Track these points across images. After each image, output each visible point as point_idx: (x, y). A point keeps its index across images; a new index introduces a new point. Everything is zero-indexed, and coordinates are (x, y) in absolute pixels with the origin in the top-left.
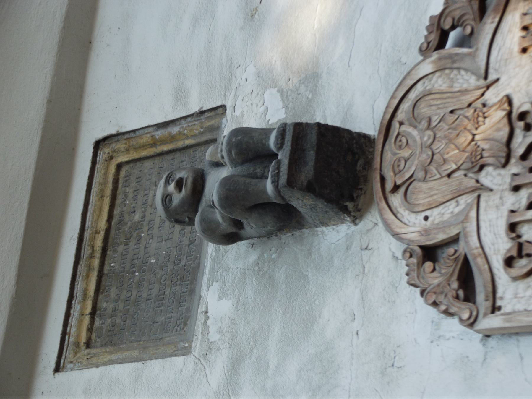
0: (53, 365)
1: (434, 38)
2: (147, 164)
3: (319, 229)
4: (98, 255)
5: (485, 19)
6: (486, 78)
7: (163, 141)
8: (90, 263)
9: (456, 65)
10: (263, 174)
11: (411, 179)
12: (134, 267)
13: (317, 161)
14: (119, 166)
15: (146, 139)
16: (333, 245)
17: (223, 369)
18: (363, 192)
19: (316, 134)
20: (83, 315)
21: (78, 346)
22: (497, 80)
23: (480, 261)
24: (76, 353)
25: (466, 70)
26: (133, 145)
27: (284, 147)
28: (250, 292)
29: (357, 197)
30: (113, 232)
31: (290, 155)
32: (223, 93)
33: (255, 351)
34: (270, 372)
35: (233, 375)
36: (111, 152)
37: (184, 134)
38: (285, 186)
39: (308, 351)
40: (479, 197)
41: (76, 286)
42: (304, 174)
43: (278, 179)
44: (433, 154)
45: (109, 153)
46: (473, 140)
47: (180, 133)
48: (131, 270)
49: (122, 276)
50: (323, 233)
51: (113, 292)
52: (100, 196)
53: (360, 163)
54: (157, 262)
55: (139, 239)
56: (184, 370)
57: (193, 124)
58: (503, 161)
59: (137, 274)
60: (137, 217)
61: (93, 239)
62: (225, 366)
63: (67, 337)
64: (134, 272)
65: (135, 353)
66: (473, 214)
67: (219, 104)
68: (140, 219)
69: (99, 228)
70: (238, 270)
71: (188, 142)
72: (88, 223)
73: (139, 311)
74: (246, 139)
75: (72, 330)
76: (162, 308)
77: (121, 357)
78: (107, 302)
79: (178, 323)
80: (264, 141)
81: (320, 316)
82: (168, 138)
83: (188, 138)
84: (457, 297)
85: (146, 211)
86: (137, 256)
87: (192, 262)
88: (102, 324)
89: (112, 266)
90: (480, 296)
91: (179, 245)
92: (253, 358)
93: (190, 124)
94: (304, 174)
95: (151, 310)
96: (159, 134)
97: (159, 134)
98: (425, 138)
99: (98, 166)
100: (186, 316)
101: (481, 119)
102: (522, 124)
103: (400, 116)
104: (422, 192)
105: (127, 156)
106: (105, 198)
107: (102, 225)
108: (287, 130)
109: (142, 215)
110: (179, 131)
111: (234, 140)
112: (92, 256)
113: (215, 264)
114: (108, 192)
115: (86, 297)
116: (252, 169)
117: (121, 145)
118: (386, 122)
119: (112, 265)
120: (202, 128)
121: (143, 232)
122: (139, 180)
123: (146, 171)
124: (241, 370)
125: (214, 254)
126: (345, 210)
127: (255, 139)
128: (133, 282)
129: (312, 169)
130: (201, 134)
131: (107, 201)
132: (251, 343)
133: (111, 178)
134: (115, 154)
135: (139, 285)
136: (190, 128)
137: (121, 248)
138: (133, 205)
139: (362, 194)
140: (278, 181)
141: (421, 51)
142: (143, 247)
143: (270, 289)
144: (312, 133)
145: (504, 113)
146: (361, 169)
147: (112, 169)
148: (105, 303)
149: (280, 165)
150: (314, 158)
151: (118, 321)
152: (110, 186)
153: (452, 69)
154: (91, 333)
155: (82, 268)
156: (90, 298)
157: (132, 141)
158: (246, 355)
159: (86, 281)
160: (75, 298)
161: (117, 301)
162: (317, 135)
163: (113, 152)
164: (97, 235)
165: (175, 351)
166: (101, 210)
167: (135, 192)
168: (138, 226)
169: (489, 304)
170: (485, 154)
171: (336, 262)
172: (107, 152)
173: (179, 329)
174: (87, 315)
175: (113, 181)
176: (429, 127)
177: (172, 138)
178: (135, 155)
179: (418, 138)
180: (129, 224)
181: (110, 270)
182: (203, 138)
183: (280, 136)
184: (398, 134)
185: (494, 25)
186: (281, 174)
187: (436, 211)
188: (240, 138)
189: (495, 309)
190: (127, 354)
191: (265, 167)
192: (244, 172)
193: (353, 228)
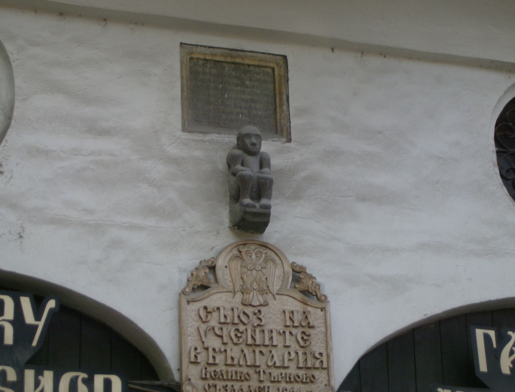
0: (183, 42)
1: (298, 269)
2: (271, 86)
4: (232, 60)
5: (300, 294)
6: (277, 294)
7: (281, 99)
9: (285, 280)
11: (242, 259)
14: (273, 69)
15: (284, 90)
22: (275, 299)
23: (207, 295)
25: (282, 285)
40: (231, 292)
44: (251, 270)
46: (254, 289)
47: (283, 111)
51: (214, 71)
58: (244, 303)
60: (248, 83)
61: (239, 56)
66: (225, 290)
72: (248, 54)
75: (199, 49)
83: (280, 115)
84: (194, 285)
90: (194, 296)
96: (284, 97)
97: (284, 97)
98: (258, 266)
101: (262, 293)
102: (256, 311)
103: (269, 252)
104: (236, 264)
107: (247, 62)
114: (262, 64)
117: (282, 73)
118: (267, 246)
125: (224, 142)
126: (234, 226)
130: (281, 124)
131: (257, 63)
133: (268, 64)
137: (234, 74)
141: (293, 263)
145: (262, 303)
147: (272, 65)
153: (284, 278)
169: (190, 300)
170: (248, 295)
176: (262, 268)
177: (281, 105)
178: (277, 80)
179: (258, 262)
180: (245, 78)
182: (278, 125)
184: (262, 253)
185: (296, 298)
187: (228, 271)
189: (188, 302)
190: (185, 89)
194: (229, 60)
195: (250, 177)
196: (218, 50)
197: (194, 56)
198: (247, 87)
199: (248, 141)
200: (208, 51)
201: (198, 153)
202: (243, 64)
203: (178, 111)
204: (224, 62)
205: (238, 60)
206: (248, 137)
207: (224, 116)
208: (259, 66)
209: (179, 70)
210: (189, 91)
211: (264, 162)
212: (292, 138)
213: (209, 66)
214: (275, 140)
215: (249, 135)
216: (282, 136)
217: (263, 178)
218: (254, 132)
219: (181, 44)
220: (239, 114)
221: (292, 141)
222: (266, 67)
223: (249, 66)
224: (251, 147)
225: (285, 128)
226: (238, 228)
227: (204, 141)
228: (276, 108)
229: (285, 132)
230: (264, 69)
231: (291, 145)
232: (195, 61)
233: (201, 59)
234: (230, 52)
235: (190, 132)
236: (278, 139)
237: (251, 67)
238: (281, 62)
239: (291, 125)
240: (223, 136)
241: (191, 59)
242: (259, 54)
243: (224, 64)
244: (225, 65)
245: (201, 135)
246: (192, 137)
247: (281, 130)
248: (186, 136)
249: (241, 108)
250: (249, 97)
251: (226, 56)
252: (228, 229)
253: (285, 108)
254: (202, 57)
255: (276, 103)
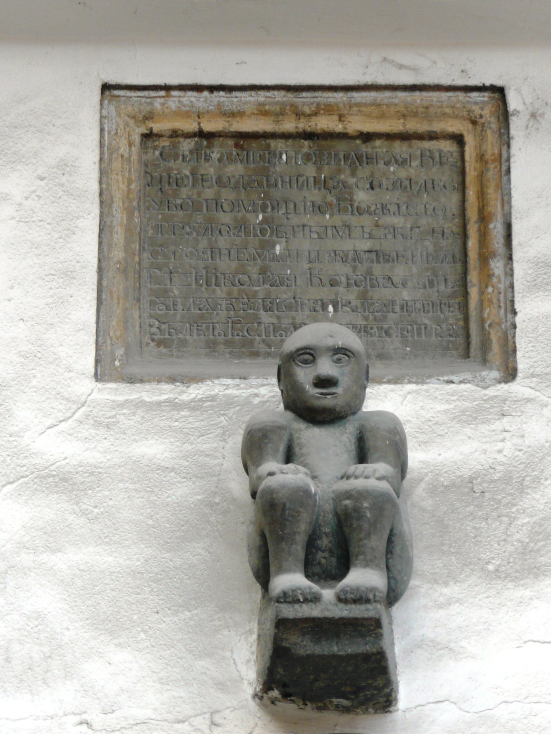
0: (113, 79)
2: (455, 198)
3: (256, 626)
4: (303, 125)
8: (287, 114)
10: (320, 549)
12: (273, 208)
13: (323, 657)
15: (495, 207)
16: (229, 654)
17: (63, 456)
18: (303, 706)
19: (365, 652)
20: (199, 117)
21: (147, 119)
24: (134, 117)
26: (488, 170)
27: (341, 605)
28: (179, 493)
29: (291, 700)
30: (342, 147)
31: (325, 618)
32: (538, 370)
33: (82, 520)
34: (44, 557)
35: (51, 479)
36: (482, 120)
37: (487, 287)
38: (277, 616)
39: (68, 629)
41: (248, 93)
42: (300, 640)
43: (289, 602)
45: (481, 116)
48: (268, 203)
49: (260, 184)
50: (251, 632)
51: (236, 170)
52: (405, 112)
53: (345, 702)
54: (275, 258)
55: (319, 209)
56: (71, 374)
57: (502, 305)
59: (261, 217)
61: (329, 109)
62: (67, 461)
63: (163, 93)
64: (264, 209)
65: (118, 254)
67: (522, 364)
68: (356, 205)
69: (350, 118)
70: (221, 460)
71: (474, 292)
72: (357, 96)
73: (195, 234)
74: (366, 526)
75: (175, 100)
76: (194, 286)
77: (115, 223)
78: (220, 160)
79: (163, 326)
80: (361, 557)
81: (119, 645)
82: (487, 249)
83: (482, 293)
85: (371, 214)
86: (292, 211)
87: (264, 337)
88: (183, 156)
89: (281, 157)
91: (296, 302)
92: (71, 518)
93: (502, 296)
94: (300, 640)
95: (193, 262)
97: (496, 228)
99: (461, 95)
100: (173, 341)
105: (474, 155)
106: (402, 121)
107: (357, 124)
108: (369, 606)
109: (364, 206)
110: (493, 275)
111: (366, 505)
112: (299, 115)
113: (238, 408)
115: (229, 117)
116: (327, 530)
119: (284, 157)
120: (490, 325)
121: (332, 215)
122: (430, 186)
123: (443, 200)
124: (55, 496)
125: (256, 401)
127: (366, 541)
128: (247, 211)
129: (308, 652)
130: (482, 321)
132: (96, 510)
133: (437, 127)
134: (479, 128)
135: (242, 226)
136: (495, 301)
137: (310, 171)
138: (384, 183)
139: (299, 706)
140: (285, 602)
142: (305, 221)
143: (178, 534)
144: (366, 644)
146: (335, 703)
148: (218, 156)
149: (311, 601)
150: (326, 653)
151: (184, 192)
152: (422, 127)
154: (171, 136)
155: (279, 96)
156: (227, 124)
157: (496, 167)
158: (77, 503)
159: (255, 111)
160: (229, 95)
161: (219, 182)
162: (363, 654)
163: (483, 124)
164: (336, 118)
165: (111, 338)
166: (382, 116)
167: (407, 183)
168: (345, 203)
171: (202, 664)
172: (483, 113)
173: (154, 330)
174: (199, 124)
175: (433, 132)
177: (485, 259)
180: (352, 181)
181: (275, 155)
183: (358, 596)
186: (297, 606)
188: (369, 515)
191: (330, 551)
192: (324, 516)
193: (250, 691)
194: (289, 125)
195: (302, 496)
196: (245, 96)
197: (157, 127)
198: (360, 211)
199: (304, 376)
200: (200, 101)
201: (155, 449)
202: (343, 136)
203: (85, 311)
204: (273, 136)
205: (324, 123)
206: (305, 362)
207: (266, 318)
208: (405, 137)
209: (95, 175)
210: (136, 246)
211: (379, 443)
212: (521, 366)
213: (215, 156)
214: (454, 378)
215: (307, 355)
216: (484, 361)
217: (348, 495)
218: (330, 342)
219: (106, 87)
220: (324, 307)
221: (520, 375)
222: (432, 136)
223: (367, 137)
224: (315, 391)
225: (495, 337)
226: (286, 696)
227: (174, 405)
228: (465, 272)
229: (496, 347)
230: (427, 145)
231: (516, 388)
232: (165, 143)
233: (188, 136)
234: (290, 97)
235: (131, 380)
236: (468, 376)
237: (378, 143)
238: (486, 112)
239: (518, 319)
240: (254, 381)
241: (148, 136)
242: (401, 95)
243: (273, 143)
244: (278, 145)
245: (166, 387)
246: (134, 396)
247: (471, 335)
248: (113, 392)
249: (333, 283)
250: (366, 245)
251: (277, 115)
252: (253, 705)
253: (497, 266)
254: (190, 126)
255: (465, 254)
